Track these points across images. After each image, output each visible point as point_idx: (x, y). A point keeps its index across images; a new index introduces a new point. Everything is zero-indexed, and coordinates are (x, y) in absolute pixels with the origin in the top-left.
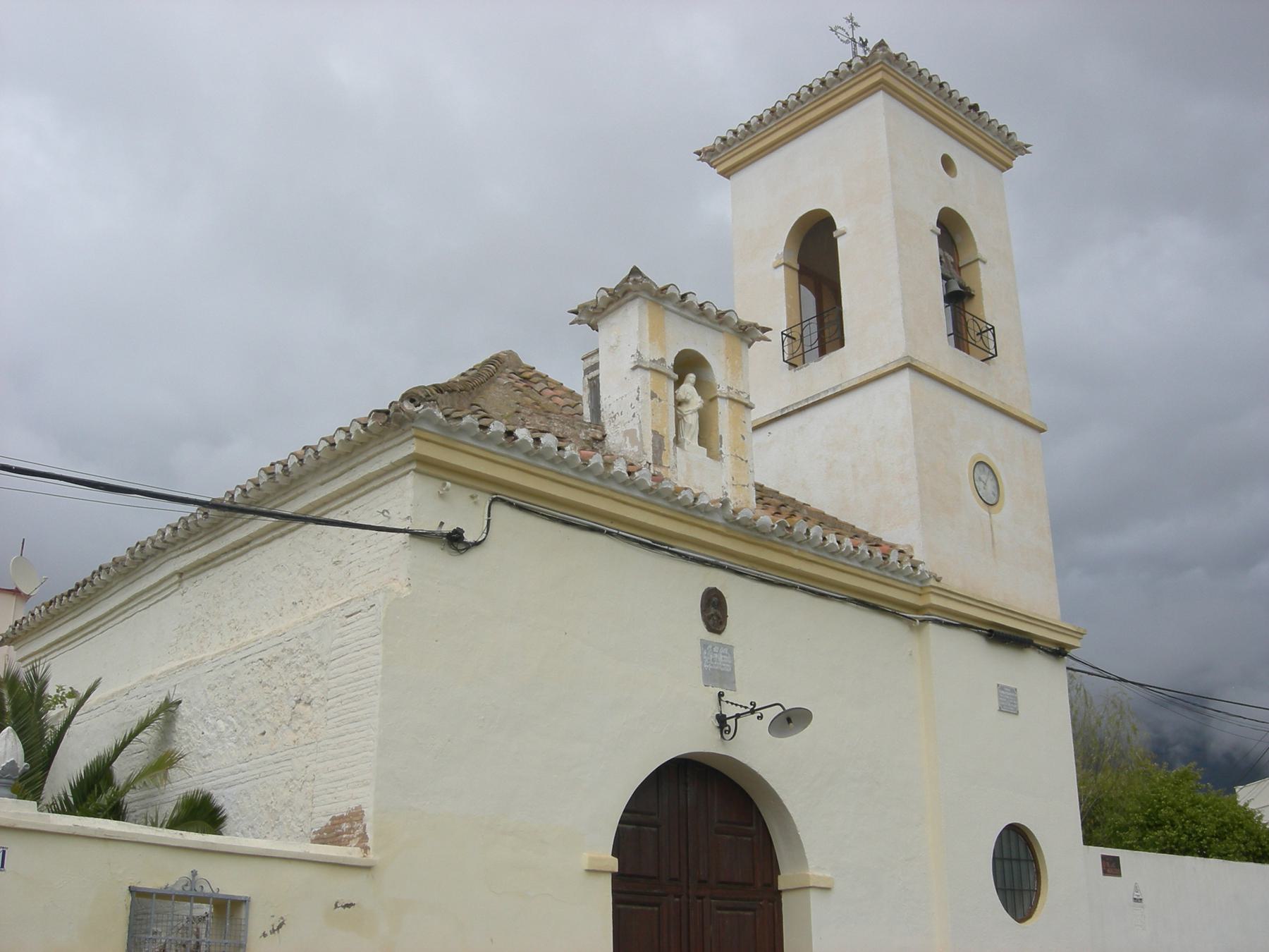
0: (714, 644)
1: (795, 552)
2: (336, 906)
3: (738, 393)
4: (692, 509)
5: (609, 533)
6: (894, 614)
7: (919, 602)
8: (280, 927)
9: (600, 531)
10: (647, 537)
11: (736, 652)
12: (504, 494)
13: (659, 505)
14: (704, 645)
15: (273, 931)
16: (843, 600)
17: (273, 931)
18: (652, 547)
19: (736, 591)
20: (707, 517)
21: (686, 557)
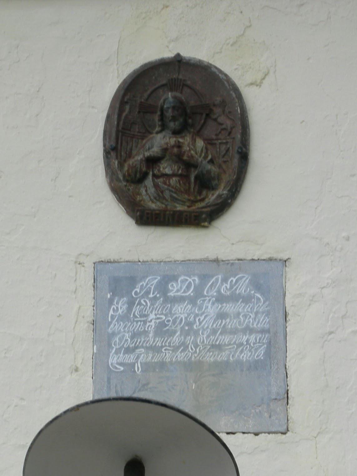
0: (168, 273)
11: (295, 283)
14: (116, 281)
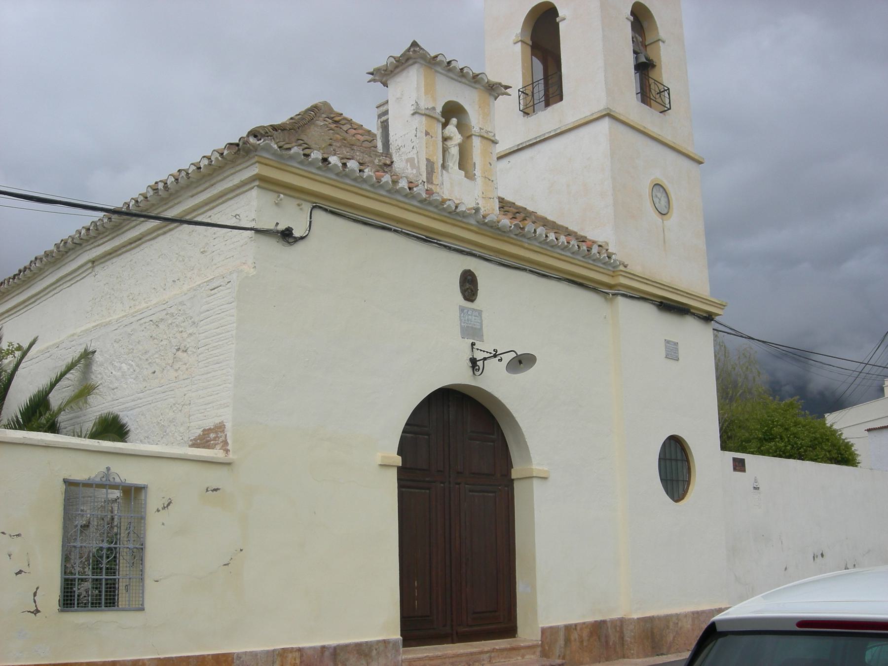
1: (526, 245)
2: (207, 490)
3: (487, 132)
4: (454, 215)
5: (395, 231)
6: (594, 290)
7: (611, 281)
8: (169, 505)
9: (389, 229)
10: (422, 234)
12: (322, 203)
13: (347, 184)
14: (462, 309)
15: (164, 508)
16: (559, 279)
17: (164, 508)
18: (426, 241)
19: (484, 272)
20: (465, 220)
21: (450, 248)
